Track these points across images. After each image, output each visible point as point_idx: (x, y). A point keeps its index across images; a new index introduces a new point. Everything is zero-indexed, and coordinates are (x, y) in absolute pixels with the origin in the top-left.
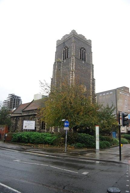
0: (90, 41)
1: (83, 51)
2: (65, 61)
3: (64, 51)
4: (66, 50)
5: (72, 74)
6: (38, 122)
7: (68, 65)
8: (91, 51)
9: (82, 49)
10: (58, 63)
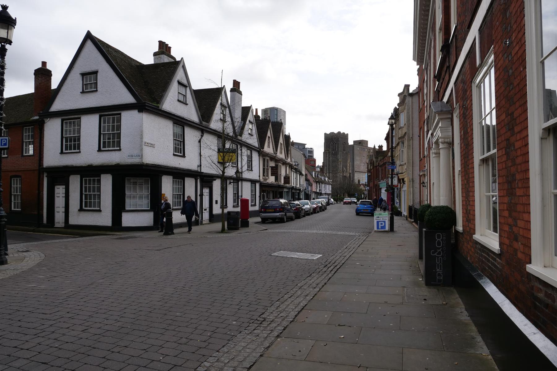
2: (334, 152)
3: (332, 144)
4: (334, 144)
5: (341, 163)
7: (337, 156)
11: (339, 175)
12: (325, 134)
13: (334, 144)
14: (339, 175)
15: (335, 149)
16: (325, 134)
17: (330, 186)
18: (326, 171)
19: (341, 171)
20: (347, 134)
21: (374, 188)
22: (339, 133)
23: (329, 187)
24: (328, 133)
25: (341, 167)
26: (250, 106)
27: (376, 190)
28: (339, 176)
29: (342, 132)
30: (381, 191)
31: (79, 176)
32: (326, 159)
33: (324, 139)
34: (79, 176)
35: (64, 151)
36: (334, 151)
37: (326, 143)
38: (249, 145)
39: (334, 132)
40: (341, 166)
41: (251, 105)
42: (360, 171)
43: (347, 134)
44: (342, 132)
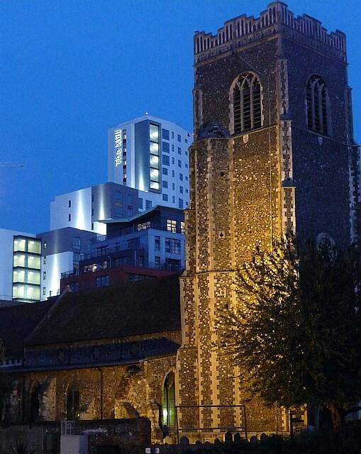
0: (341, 35)
1: (316, 88)
4: (246, 85)
6: (152, 395)
8: (346, 82)
9: (313, 80)
10: (214, 145)
18: (204, 261)
36: (247, 128)
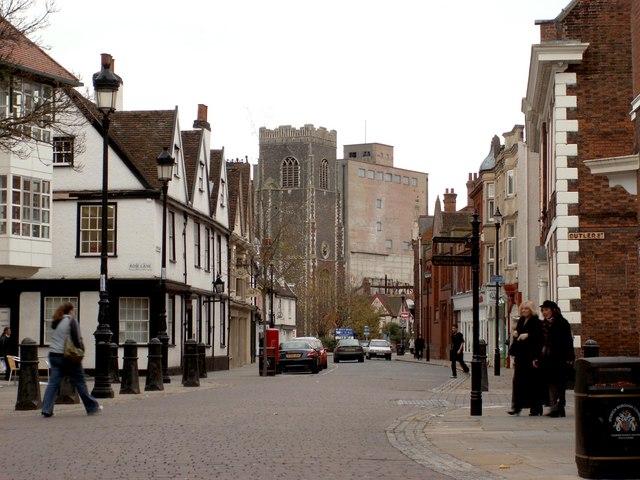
2: (289, 191)
3: (285, 164)
4: (291, 163)
11: (308, 265)
12: (263, 131)
13: (291, 163)
14: (308, 265)
15: (296, 178)
16: (263, 131)
17: (293, 303)
19: (313, 253)
20: (334, 132)
21: (435, 311)
22: (308, 128)
23: (189, 312)
24: (272, 126)
25: (313, 240)
26: (173, 108)
27: (444, 315)
28: (309, 270)
29: (317, 127)
30: (456, 319)
31: (39, 294)
32: (265, 212)
33: (258, 148)
34: (39, 294)
35: (81, 254)
37: (266, 160)
38: (174, 204)
39: (293, 126)
40: (313, 236)
41: (177, 107)
42: (367, 250)
43: (334, 132)
44: (317, 127)
